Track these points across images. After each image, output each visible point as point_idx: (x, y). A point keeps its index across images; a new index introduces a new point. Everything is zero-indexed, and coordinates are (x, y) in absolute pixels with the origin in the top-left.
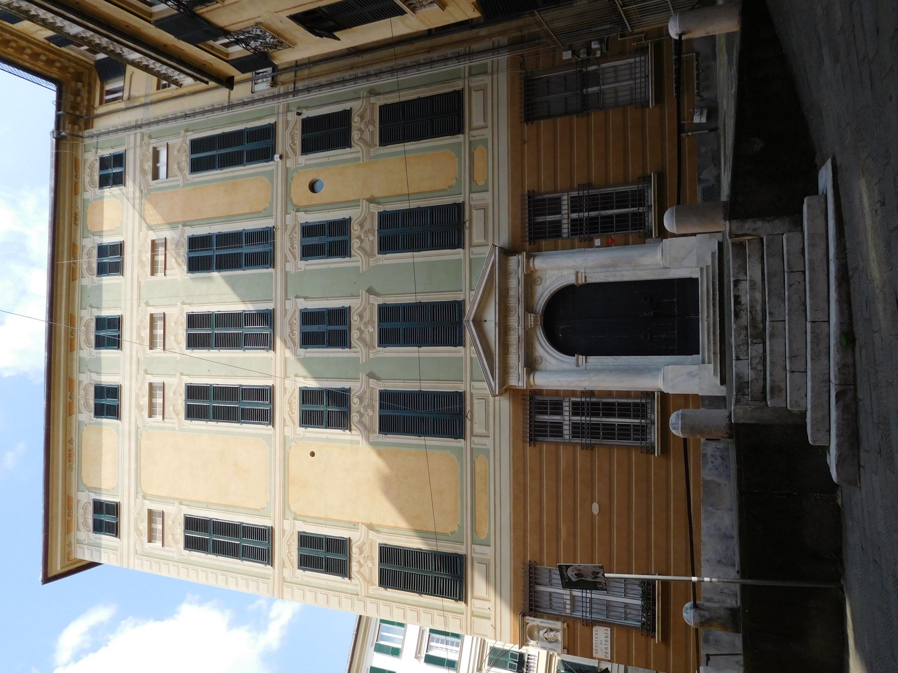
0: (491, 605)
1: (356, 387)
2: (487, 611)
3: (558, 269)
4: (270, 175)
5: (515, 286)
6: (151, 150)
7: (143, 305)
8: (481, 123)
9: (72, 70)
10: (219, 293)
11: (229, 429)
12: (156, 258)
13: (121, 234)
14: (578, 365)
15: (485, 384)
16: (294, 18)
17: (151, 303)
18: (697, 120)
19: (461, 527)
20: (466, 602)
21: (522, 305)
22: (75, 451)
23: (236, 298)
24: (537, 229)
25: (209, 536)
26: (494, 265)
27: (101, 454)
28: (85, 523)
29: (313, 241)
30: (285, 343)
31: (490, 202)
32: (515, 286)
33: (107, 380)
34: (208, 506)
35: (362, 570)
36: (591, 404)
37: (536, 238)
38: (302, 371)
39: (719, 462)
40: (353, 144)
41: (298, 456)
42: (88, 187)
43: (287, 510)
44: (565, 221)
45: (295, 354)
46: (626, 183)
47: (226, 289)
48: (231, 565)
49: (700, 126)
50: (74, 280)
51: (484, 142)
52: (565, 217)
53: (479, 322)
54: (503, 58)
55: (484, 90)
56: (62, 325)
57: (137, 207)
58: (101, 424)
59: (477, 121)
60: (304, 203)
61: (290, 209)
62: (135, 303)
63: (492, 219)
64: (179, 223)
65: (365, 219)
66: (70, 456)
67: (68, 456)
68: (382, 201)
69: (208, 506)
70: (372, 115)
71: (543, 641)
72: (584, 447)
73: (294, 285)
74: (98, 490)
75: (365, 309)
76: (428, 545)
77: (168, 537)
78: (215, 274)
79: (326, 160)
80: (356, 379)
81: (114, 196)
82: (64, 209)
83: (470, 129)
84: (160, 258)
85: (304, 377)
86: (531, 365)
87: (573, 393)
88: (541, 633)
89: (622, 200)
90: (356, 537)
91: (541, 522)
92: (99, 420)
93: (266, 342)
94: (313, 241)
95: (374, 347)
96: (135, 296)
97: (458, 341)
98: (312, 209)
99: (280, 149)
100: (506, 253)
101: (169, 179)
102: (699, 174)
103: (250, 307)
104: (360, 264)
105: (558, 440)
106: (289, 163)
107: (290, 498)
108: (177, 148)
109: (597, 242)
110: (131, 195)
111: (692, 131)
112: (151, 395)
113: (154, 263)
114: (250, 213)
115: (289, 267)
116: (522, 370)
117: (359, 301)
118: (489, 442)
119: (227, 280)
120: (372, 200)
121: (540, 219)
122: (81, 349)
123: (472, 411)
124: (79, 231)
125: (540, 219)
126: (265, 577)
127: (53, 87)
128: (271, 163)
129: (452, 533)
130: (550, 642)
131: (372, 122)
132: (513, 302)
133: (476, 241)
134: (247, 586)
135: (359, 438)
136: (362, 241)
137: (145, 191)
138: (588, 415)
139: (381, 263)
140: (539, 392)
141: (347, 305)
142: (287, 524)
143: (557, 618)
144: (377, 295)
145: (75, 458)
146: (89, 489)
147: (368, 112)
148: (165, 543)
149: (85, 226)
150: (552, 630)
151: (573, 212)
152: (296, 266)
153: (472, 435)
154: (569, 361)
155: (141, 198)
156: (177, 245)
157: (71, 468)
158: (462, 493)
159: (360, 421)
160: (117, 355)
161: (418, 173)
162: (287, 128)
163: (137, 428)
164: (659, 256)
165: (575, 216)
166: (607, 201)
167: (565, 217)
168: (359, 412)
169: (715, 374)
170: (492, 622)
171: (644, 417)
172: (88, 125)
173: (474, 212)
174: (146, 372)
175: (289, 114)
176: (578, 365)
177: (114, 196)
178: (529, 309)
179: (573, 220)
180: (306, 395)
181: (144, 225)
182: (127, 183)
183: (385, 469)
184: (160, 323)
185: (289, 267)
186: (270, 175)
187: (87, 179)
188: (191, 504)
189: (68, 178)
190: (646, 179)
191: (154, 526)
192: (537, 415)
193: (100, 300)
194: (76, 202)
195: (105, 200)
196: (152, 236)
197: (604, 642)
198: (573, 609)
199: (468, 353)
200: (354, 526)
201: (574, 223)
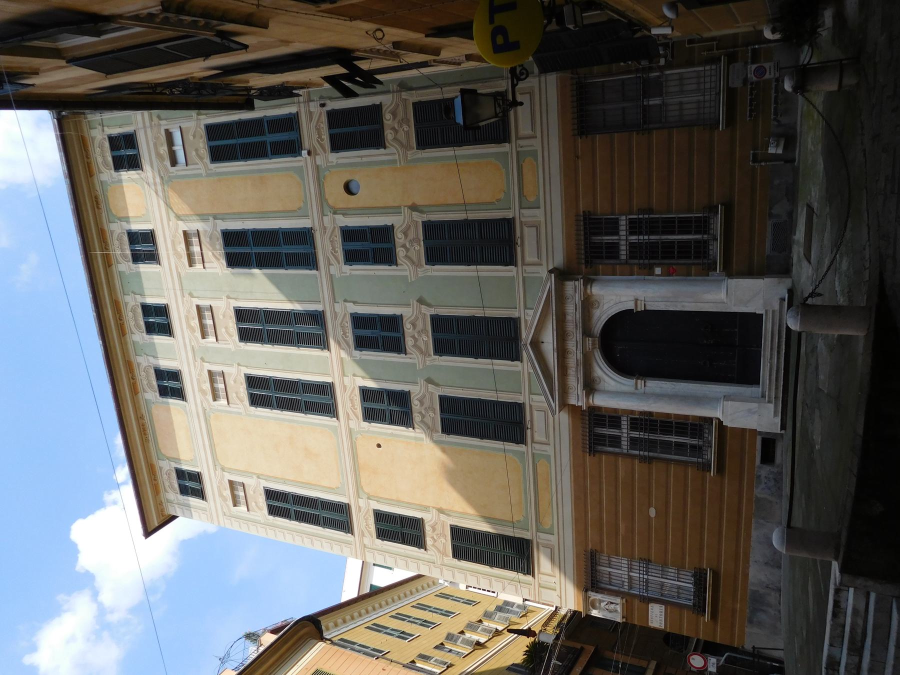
0: (557, 579)
1: (416, 390)
2: (554, 585)
3: (616, 296)
4: (299, 171)
5: (573, 311)
7: (187, 296)
10: (262, 290)
11: (295, 418)
12: (204, 321)
13: (149, 221)
14: (636, 388)
15: (543, 398)
17: (195, 294)
18: (772, 150)
19: (526, 517)
20: (533, 576)
21: (580, 331)
22: (148, 425)
23: (282, 297)
24: (592, 252)
25: (282, 504)
27: (174, 430)
28: (137, 326)
30: (339, 344)
31: (543, 220)
32: (573, 311)
33: (166, 364)
34: (285, 481)
35: (436, 544)
38: (359, 372)
39: (772, 483)
40: (387, 144)
41: (366, 448)
43: (361, 492)
44: (623, 233)
45: (351, 355)
46: (690, 211)
47: (271, 288)
48: (315, 531)
49: (775, 157)
50: (110, 265)
51: (534, 154)
53: (536, 344)
56: (109, 312)
57: (160, 193)
58: (168, 403)
59: (524, 128)
60: (341, 205)
61: (327, 210)
62: (179, 293)
63: (545, 238)
64: (209, 215)
65: (408, 227)
66: (144, 430)
67: (143, 430)
68: (425, 209)
69: (285, 481)
70: (406, 113)
72: (643, 459)
73: (338, 288)
74: (177, 460)
75: (417, 318)
77: (221, 331)
78: (256, 271)
79: (359, 160)
80: (415, 383)
81: (133, 180)
82: (84, 196)
83: (517, 138)
84: (196, 249)
85: (363, 378)
86: (590, 386)
88: (603, 604)
89: (684, 226)
90: (429, 518)
91: (601, 518)
92: (165, 400)
93: (321, 342)
94: (367, 333)
95: (430, 355)
96: (177, 287)
97: (515, 356)
98: (351, 212)
99: (306, 144)
100: (562, 275)
101: (189, 167)
102: (771, 209)
103: (297, 307)
104: (407, 273)
105: (617, 450)
106: (319, 160)
107: (362, 480)
108: (191, 132)
109: (658, 271)
110: (151, 181)
111: (766, 162)
112: (188, 244)
113: (203, 327)
114: (284, 211)
117: (411, 310)
118: (549, 450)
120: (414, 208)
121: (597, 239)
122: (118, 263)
123: (532, 421)
124: (104, 215)
125: (597, 239)
126: (347, 543)
128: (298, 158)
130: (610, 612)
131: (405, 120)
132: (570, 327)
133: (528, 259)
134: (332, 548)
135: (423, 436)
136: (407, 250)
137: (166, 178)
138: (646, 234)
139: (429, 274)
140: (599, 408)
141: (398, 313)
142: (362, 503)
143: (616, 593)
144: (429, 305)
145: (149, 431)
146: (120, 219)
147: (401, 108)
148: (219, 338)
149: (109, 211)
150: (612, 603)
151: (631, 234)
152: (327, 159)
153: (533, 441)
154: (627, 384)
155: (163, 184)
156: (211, 238)
157: (147, 440)
159: (422, 421)
160: (171, 342)
161: (460, 181)
162: (311, 121)
163: (204, 410)
164: (722, 296)
165: (633, 238)
166: (669, 226)
168: (393, 129)
169: (775, 415)
170: (558, 592)
171: (701, 437)
173: (526, 229)
174: (203, 360)
175: (311, 104)
176: (636, 388)
177: (133, 180)
178: (587, 332)
180: (366, 394)
181: (172, 216)
182: (144, 167)
183: (451, 465)
184: (195, 240)
185: (334, 270)
186: (299, 171)
188: (268, 478)
189: (105, 286)
190: (713, 209)
191: (236, 493)
193: (141, 287)
194: (93, 184)
195: (124, 184)
196: (183, 226)
198: (630, 587)
199: (524, 367)
200: (426, 509)
201: (632, 246)
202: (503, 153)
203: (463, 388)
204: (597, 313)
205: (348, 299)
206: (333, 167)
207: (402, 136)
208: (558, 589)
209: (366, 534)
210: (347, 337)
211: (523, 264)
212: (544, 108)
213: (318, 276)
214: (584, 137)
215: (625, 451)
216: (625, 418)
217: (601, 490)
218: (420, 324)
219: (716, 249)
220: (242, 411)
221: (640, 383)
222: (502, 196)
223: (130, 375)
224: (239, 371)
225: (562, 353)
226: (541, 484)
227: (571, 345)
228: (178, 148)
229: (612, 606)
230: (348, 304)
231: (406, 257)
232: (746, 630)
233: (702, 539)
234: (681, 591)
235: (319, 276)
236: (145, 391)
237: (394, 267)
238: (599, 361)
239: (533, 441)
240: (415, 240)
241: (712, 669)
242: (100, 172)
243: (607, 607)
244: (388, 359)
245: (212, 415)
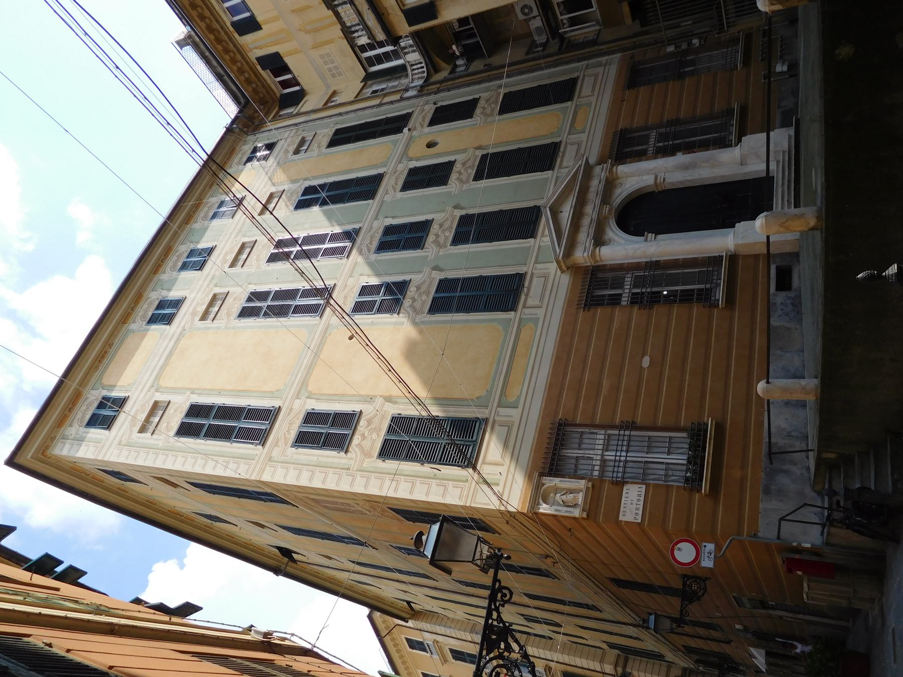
3: (637, 176)
5: (596, 185)
6: (300, 138)
8: (537, 303)
9: (261, 95)
16: (200, 609)
19: (489, 392)
22: (109, 356)
26: (580, 166)
29: (389, 238)
32: (596, 185)
36: (654, 270)
37: (591, 305)
38: (367, 270)
42: (138, 319)
48: (218, 449)
52: (626, 292)
55: (596, 76)
56: (159, 251)
66: (103, 357)
71: (559, 505)
76: (444, 411)
83: (524, 307)
85: (368, 276)
87: (636, 267)
106: (414, 133)
112: (152, 413)
116: (590, 243)
119: (325, 213)
127: (233, 109)
129: (478, 398)
132: (591, 196)
135: (405, 320)
141: (358, 410)
145: (105, 361)
149: (101, 378)
157: (97, 368)
158: (499, 360)
167: (626, 292)
173: (535, 280)
178: (606, 198)
179: (633, 294)
187: (79, 416)
192: (595, 288)
197: (635, 502)
201: (621, 287)
203: (466, 269)
204: (618, 191)
207: (418, 305)
212: (538, 359)
219: (720, 295)
223: (71, 406)
225: (578, 215)
226: (520, 349)
229: (570, 497)
232: (761, 505)
233: (704, 384)
234: (670, 473)
238: (613, 228)
241: (707, 563)
243: (564, 498)
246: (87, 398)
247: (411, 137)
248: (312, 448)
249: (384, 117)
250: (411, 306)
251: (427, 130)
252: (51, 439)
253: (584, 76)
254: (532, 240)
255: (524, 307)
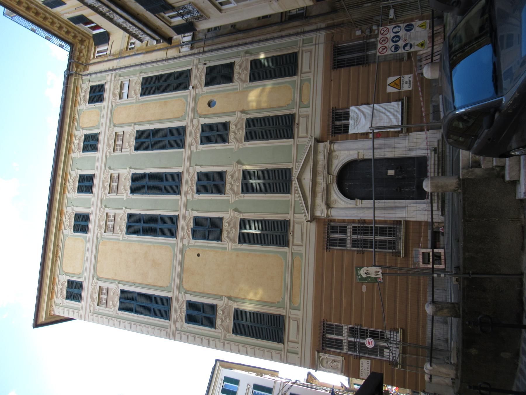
4: (186, 97)
5: (321, 158)
7: (107, 168)
14: (357, 205)
19: (283, 299)
31: (310, 113)
32: (321, 158)
36: (362, 228)
37: (335, 133)
43: (181, 288)
44: (345, 335)
54: (322, 35)
55: (311, 52)
59: (306, 68)
63: (311, 122)
64: (132, 123)
66: (57, 254)
79: (219, 89)
83: (301, 73)
86: (328, 206)
87: (354, 221)
90: (226, 216)
95: (239, 194)
99: (193, 83)
104: (234, 147)
106: (198, 91)
108: (120, 216)
115: (193, 148)
116: (324, 207)
123: (293, 232)
126: (165, 327)
128: (187, 91)
133: (301, 134)
136: (236, 134)
140: (334, 221)
141: (224, 170)
145: (60, 256)
154: (350, 203)
163: (97, 238)
165: (355, 237)
168: (239, 73)
172: (87, 66)
174: (105, 207)
185: (193, 148)
192: (331, 232)
197: (366, 369)
199: (294, 197)
202: (284, 252)
205: (195, 209)
206: (191, 246)
207: (243, 76)
208: (300, 353)
209: (179, 320)
210: (201, 81)
211: (298, 137)
213: (184, 152)
214: (335, 70)
215: (345, 352)
216: (349, 227)
217: (332, 275)
218: (236, 176)
219: (401, 247)
220: (120, 238)
221: (359, 201)
222: (290, 102)
224: (118, 287)
225: (314, 184)
226: (295, 274)
227: (320, 179)
228: (125, 91)
230: (197, 167)
231: (235, 138)
235: (184, 152)
236: (65, 229)
237: (213, 329)
239: (293, 245)
240: (241, 128)
242: (80, 104)
243: (331, 364)
244: (213, 198)
245: (101, 241)
246: (59, 281)
247: (196, 94)
248: (197, 325)
249: (172, 71)
250: (235, 138)
251: (206, 89)
252: (49, 305)
253: (302, 51)
254: (296, 77)
255: (301, 73)
